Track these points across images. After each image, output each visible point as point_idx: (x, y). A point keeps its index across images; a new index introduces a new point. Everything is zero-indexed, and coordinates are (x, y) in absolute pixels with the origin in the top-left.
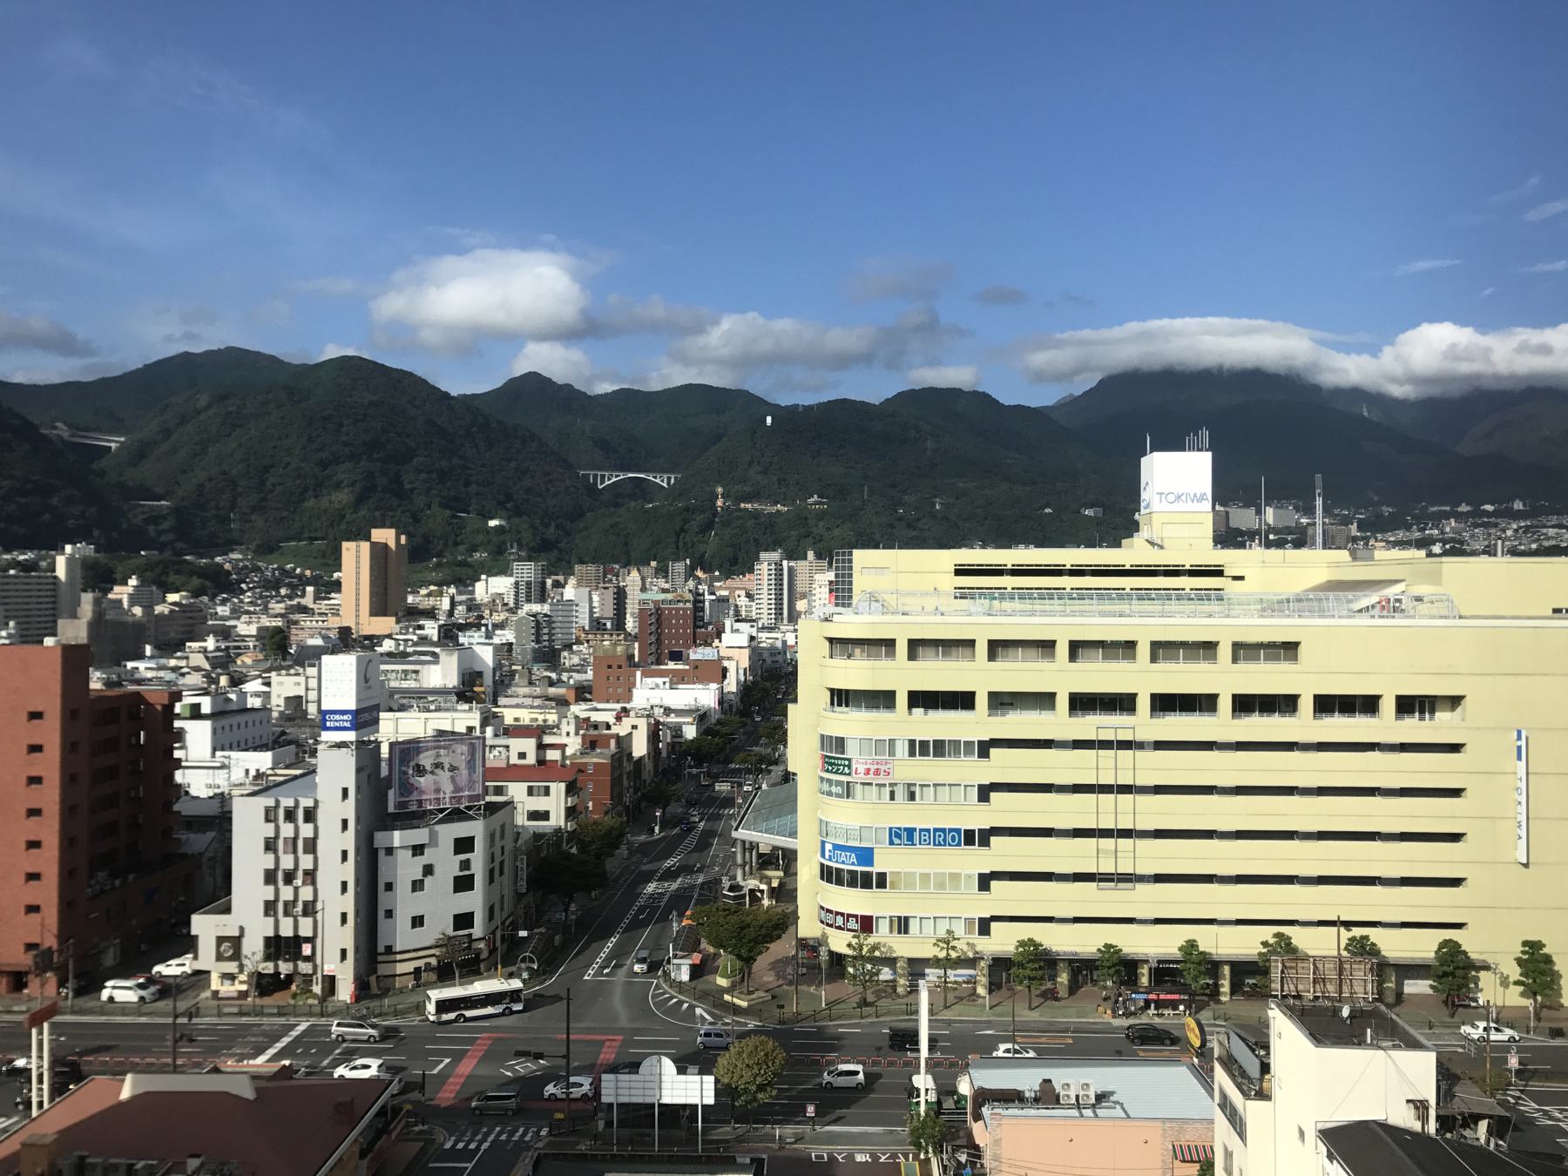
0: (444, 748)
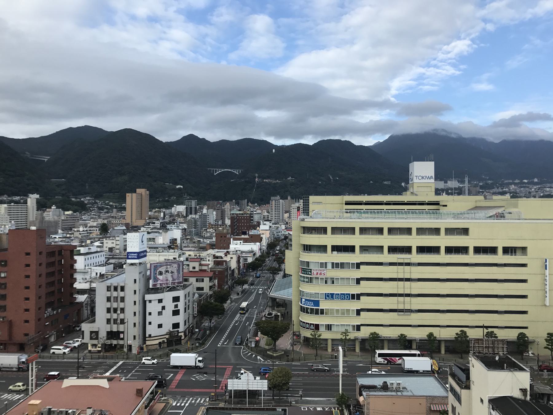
0: (169, 265)
